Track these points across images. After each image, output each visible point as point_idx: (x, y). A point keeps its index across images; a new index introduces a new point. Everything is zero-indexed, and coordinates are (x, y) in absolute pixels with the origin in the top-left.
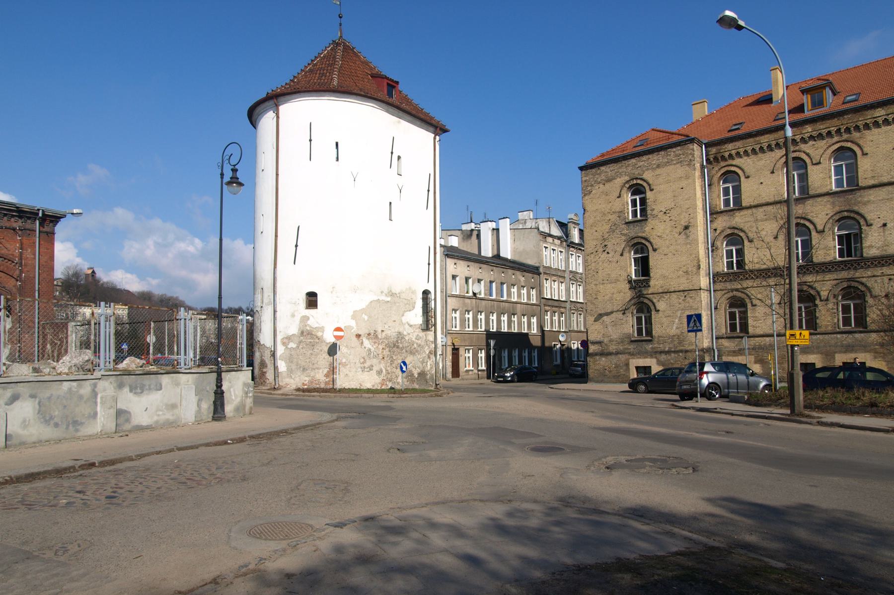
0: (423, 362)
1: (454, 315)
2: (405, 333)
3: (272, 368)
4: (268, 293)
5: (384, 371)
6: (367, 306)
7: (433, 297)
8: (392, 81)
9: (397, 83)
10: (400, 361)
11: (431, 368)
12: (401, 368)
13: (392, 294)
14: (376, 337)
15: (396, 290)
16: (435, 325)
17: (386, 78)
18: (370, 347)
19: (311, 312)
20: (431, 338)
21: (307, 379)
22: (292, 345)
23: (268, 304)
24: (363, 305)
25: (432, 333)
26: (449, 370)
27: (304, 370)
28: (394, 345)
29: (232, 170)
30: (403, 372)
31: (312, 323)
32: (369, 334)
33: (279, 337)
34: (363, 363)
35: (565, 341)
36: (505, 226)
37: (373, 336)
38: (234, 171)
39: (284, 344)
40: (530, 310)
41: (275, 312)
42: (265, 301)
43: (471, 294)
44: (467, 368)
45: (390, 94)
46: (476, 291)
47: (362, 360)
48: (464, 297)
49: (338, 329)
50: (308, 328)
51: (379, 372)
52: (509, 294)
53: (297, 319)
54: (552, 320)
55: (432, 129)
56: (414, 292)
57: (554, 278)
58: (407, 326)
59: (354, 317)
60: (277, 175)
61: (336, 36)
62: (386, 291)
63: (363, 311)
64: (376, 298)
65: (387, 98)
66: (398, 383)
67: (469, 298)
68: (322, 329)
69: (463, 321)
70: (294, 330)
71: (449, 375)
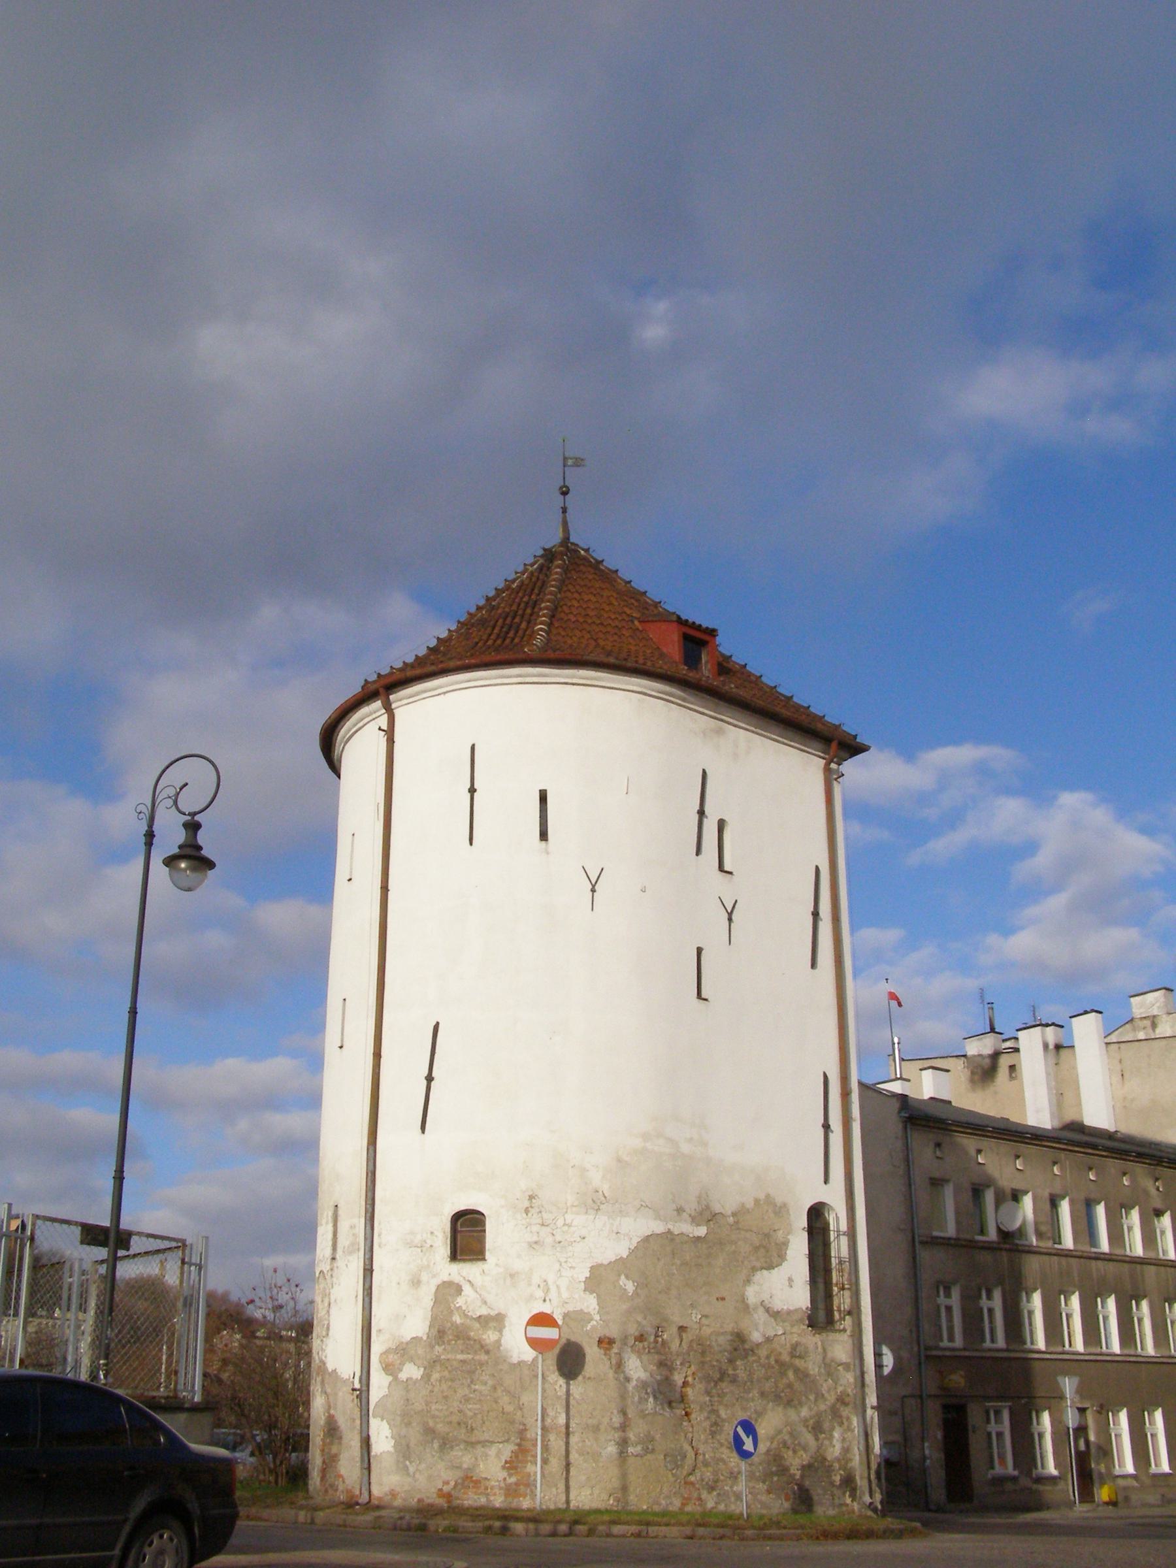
1: (942, 1300)
4: (352, 1223)
6: (632, 1252)
8: (698, 628)
9: (712, 633)
12: (738, 1443)
15: (726, 1204)
16: (854, 1311)
17: (680, 622)
22: (412, 1371)
23: (351, 1250)
24: (622, 1249)
27: (446, 1444)
28: (723, 1375)
29: (186, 825)
30: (745, 1455)
31: (468, 1301)
32: (641, 1338)
33: (377, 1349)
36: (1086, 1032)
38: (193, 827)
39: (388, 1368)
41: (369, 1271)
42: (343, 1241)
45: (692, 660)
48: (971, 1245)
50: (457, 1319)
52: (1116, 1235)
53: (427, 1295)
55: (820, 746)
56: (781, 1210)
58: (760, 1316)
60: (385, 889)
61: (553, 539)
62: (692, 1206)
63: (620, 1266)
64: (658, 1227)
65: (683, 670)
66: (738, 1497)
67: (988, 1247)
68: (497, 1321)
70: (416, 1325)
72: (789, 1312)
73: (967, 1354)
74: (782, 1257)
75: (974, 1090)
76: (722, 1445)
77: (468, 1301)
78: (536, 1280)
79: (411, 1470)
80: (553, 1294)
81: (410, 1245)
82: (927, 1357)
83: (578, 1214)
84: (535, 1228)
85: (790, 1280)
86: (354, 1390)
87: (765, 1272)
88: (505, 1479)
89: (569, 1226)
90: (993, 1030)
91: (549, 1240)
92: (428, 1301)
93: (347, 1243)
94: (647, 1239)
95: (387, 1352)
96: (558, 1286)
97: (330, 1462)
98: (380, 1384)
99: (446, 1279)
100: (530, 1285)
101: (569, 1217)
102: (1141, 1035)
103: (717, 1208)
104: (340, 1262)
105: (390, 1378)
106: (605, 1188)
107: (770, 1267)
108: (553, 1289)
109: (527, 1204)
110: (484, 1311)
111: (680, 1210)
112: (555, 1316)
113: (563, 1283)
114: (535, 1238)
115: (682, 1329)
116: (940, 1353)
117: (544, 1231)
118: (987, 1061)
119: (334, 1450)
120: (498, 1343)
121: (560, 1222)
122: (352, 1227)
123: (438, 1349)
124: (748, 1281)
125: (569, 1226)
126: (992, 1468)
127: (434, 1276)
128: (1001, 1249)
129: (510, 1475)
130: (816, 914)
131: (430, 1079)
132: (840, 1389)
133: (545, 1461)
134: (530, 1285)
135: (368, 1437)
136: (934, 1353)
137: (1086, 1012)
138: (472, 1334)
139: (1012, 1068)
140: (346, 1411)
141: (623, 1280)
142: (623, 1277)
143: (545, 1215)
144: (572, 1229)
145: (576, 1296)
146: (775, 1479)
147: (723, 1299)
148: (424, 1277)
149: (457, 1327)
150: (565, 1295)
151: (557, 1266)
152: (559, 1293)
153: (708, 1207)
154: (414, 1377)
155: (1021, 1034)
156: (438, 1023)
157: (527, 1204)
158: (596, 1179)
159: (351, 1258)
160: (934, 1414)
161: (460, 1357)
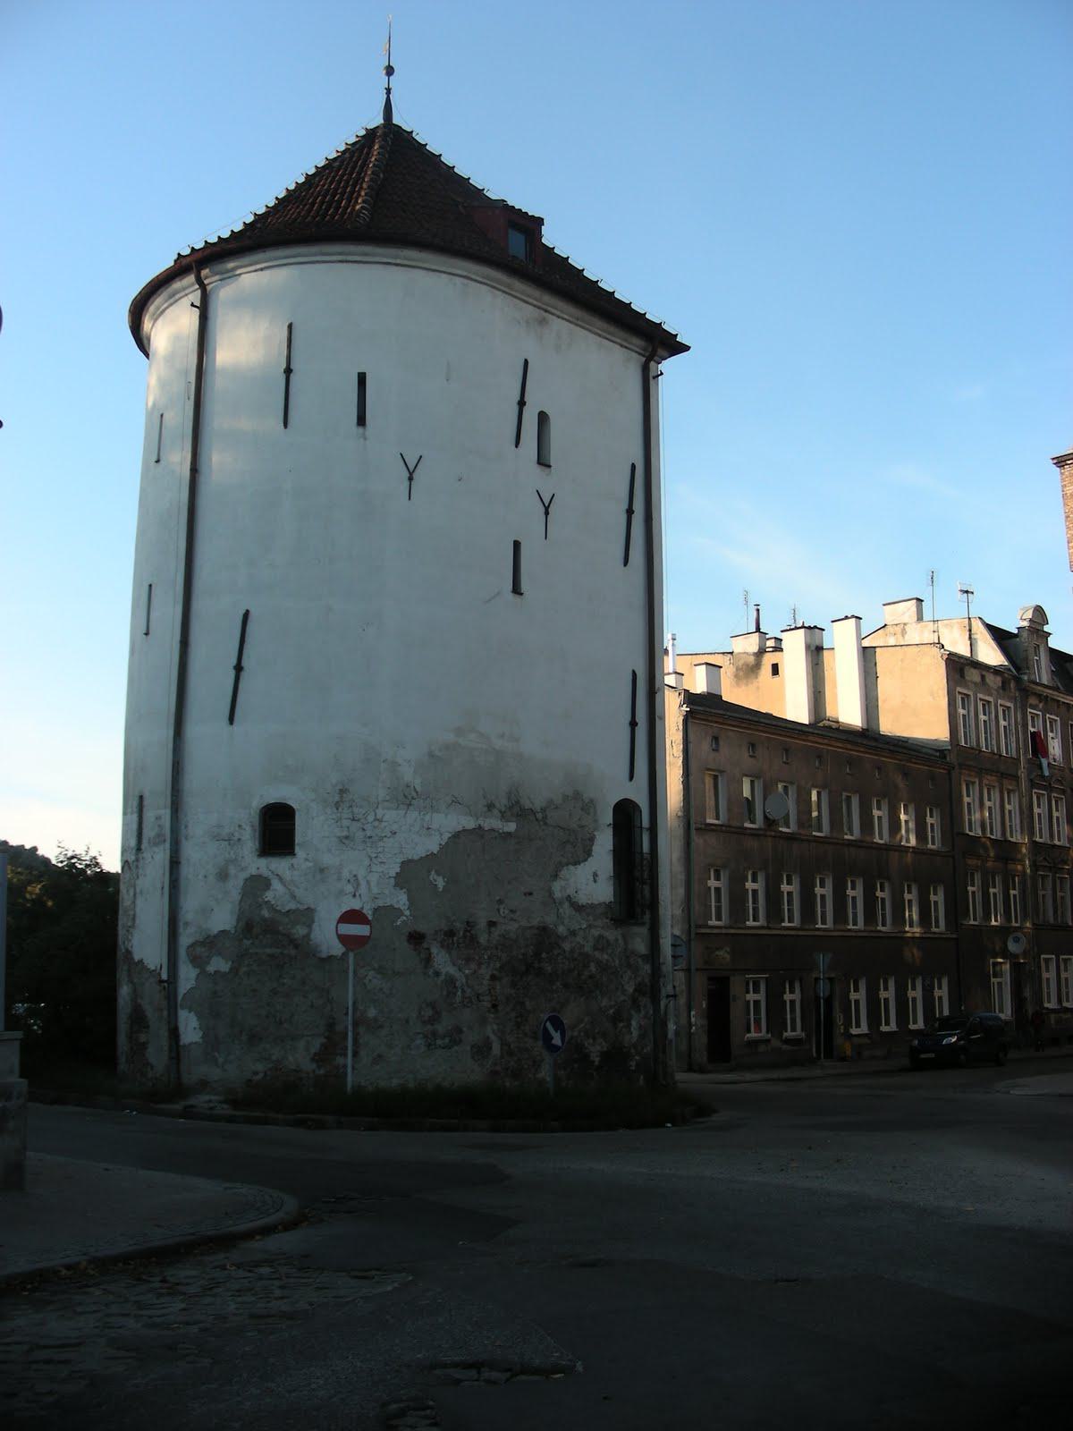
0: (616, 1019)
2: (561, 930)
3: (164, 1033)
5: (496, 1049)
6: (443, 848)
7: (646, 822)
10: (544, 1016)
11: (642, 1036)
12: (547, 1038)
13: (517, 809)
14: (471, 939)
15: (536, 798)
18: (452, 970)
19: (279, 865)
20: (640, 946)
21: (260, 1067)
22: (219, 964)
23: (158, 840)
24: (432, 845)
25: (644, 931)
26: (701, 1040)
30: (553, 1049)
31: (276, 894)
32: (451, 933)
33: (185, 940)
34: (433, 1020)
35: (1025, 954)
37: (461, 938)
39: (196, 961)
40: (925, 871)
41: (175, 863)
43: (759, 823)
44: (753, 1035)
46: (774, 814)
47: (429, 1013)
48: (743, 831)
49: (352, 916)
50: (266, 913)
51: (482, 1050)
53: (235, 886)
54: (986, 895)
56: (589, 807)
57: (988, 779)
58: (566, 910)
59: (401, 880)
62: (502, 802)
64: (470, 823)
67: (754, 834)
68: (307, 916)
69: (738, 899)
70: (223, 919)
71: (701, 1056)
72: (592, 906)
73: (732, 931)
74: (588, 853)
75: (738, 684)
76: (526, 1035)
77: (276, 894)
78: (346, 874)
79: (221, 1060)
80: (363, 889)
81: (217, 838)
82: (697, 934)
83: (388, 809)
84: (346, 823)
85: (595, 875)
86: (161, 981)
87: (571, 867)
88: (314, 1071)
89: (380, 821)
90: (758, 629)
91: (360, 835)
92: (235, 895)
93: (152, 834)
94: (456, 836)
95: (193, 945)
96: (368, 882)
97: (139, 1049)
98: (188, 976)
99: (254, 872)
100: (339, 879)
101: (380, 812)
102: (892, 641)
103: (527, 805)
104: (147, 855)
105: (197, 971)
106: (417, 783)
107: (576, 863)
108: (363, 883)
109: (337, 798)
110: (292, 906)
111: (490, 806)
112: (364, 911)
113: (374, 878)
114: (345, 833)
115: (492, 924)
116: (708, 931)
117: (355, 826)
118: (752, 659)
119: (143, 1038)
120: (308, 935)
121: (371, 818)
122: (158, 818)
123: (247, 942)
124: (555, 876)
125: (380, 821)
126: (749, 1031)
127: (243, 870)
128: (766, 836)
129: (319, 1067)
130: (630, 512)
131: (239, 668)
132: (639, 979)
133: (355, 1054)
134: (339, 879)
135: (176, 1028)
136: (703, 931)
137: (846, 618)
138: (281, 928)
139: (775, 669)
140: (152, 1000)
141: (433, 875)
142: (433, 873)
143: (356, 810)
144: (384, 824)
145: (387, 892)
146: (576, 1066)
147: (531, 894)
148: (232, 870)
149: (265, 920)
150: (375, 890)
151: (367, 862)
152: (369, 889)
153: (518, 802)
154: (222, 970)
155: (783, 636)
156: (516, 447)
157: (337, 798)
158: (408, 774)
159: (156, 849)
160: (700, 982)
161: (269, 951)
